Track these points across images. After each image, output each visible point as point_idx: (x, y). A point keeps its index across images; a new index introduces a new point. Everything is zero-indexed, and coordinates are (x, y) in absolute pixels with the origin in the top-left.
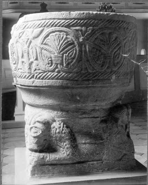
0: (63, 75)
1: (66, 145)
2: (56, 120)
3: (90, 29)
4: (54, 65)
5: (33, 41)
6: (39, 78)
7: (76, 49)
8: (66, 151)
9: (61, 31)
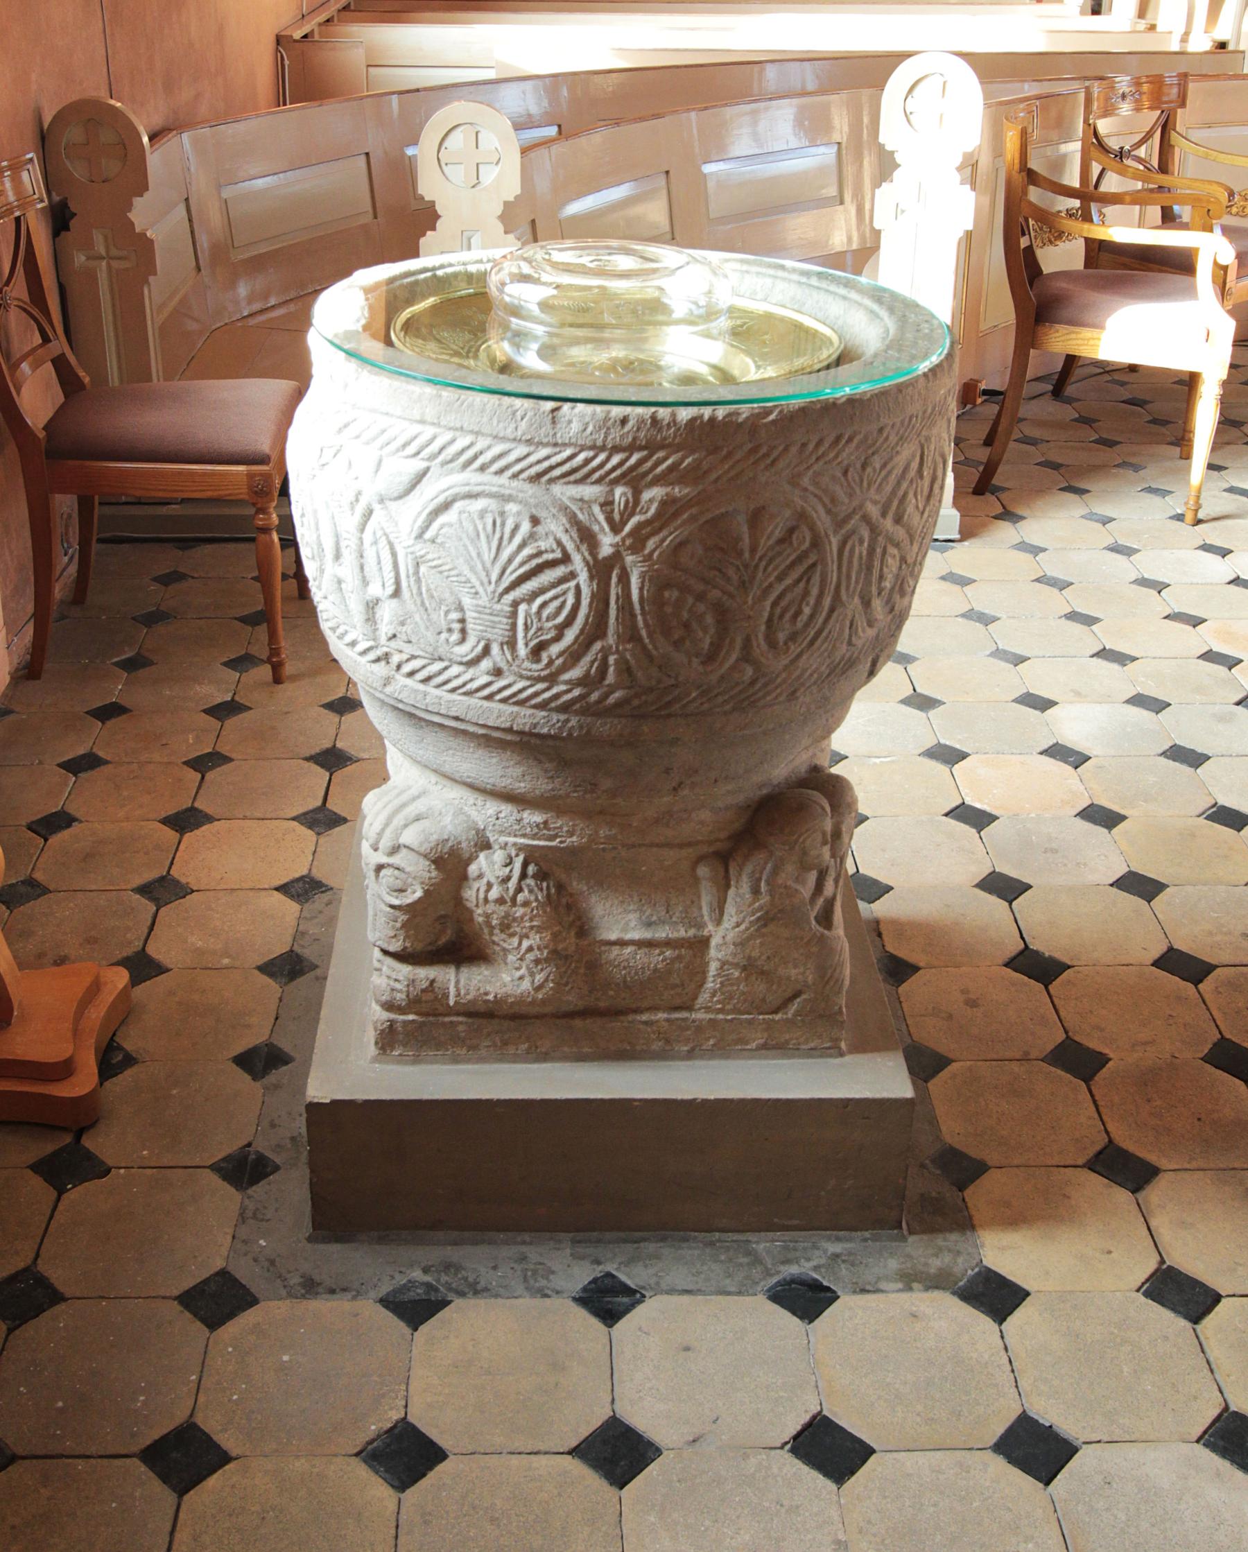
1: (530, 949)
2: (492, 840)
3: (651, 501)
7: (578, 588)
8: (528, 968)
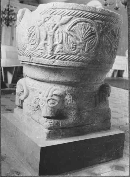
0: (83, 58)
4: (77, 49)
5: (60, 27)
6: (61, 59)
9: (86, 22)
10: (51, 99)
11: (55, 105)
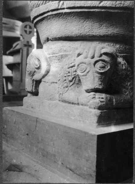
10: (100, 60)
11: (106, 70)
